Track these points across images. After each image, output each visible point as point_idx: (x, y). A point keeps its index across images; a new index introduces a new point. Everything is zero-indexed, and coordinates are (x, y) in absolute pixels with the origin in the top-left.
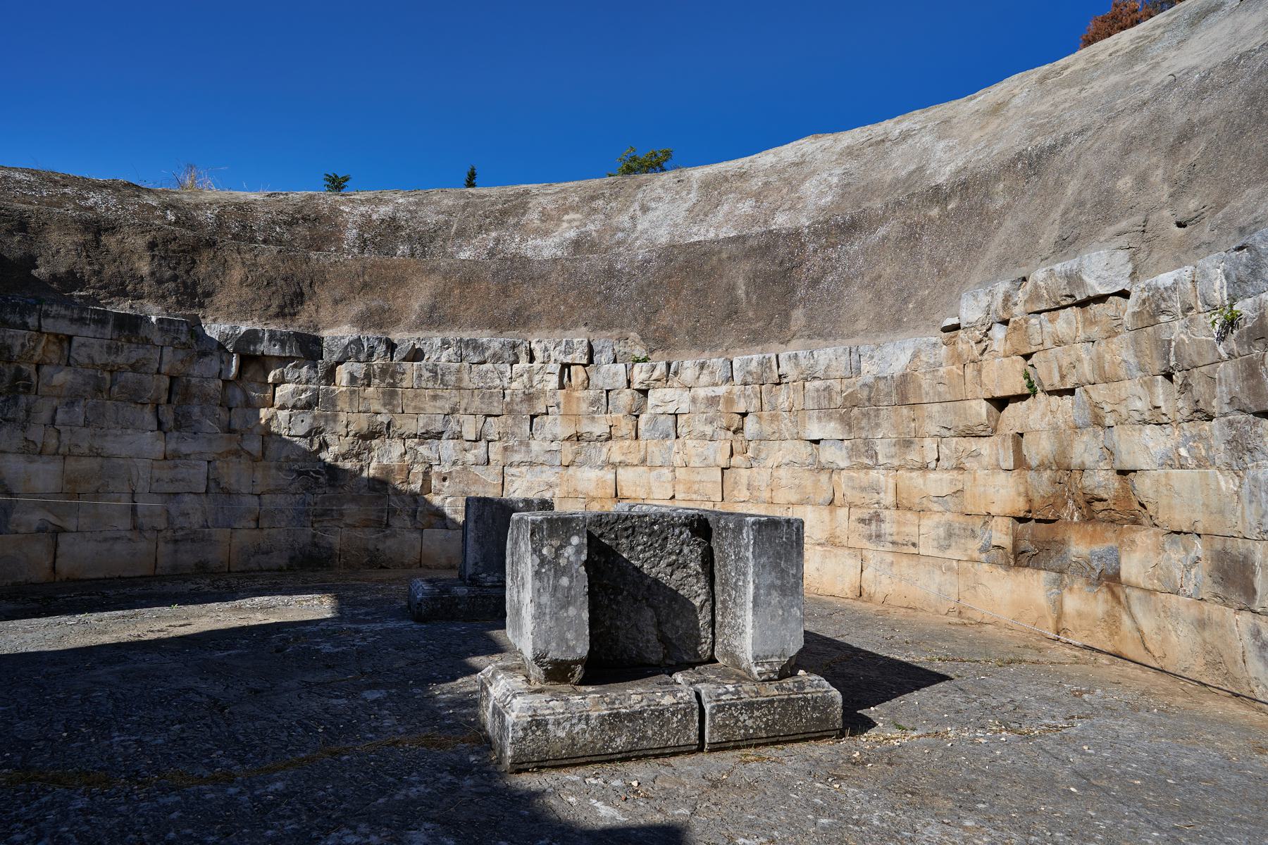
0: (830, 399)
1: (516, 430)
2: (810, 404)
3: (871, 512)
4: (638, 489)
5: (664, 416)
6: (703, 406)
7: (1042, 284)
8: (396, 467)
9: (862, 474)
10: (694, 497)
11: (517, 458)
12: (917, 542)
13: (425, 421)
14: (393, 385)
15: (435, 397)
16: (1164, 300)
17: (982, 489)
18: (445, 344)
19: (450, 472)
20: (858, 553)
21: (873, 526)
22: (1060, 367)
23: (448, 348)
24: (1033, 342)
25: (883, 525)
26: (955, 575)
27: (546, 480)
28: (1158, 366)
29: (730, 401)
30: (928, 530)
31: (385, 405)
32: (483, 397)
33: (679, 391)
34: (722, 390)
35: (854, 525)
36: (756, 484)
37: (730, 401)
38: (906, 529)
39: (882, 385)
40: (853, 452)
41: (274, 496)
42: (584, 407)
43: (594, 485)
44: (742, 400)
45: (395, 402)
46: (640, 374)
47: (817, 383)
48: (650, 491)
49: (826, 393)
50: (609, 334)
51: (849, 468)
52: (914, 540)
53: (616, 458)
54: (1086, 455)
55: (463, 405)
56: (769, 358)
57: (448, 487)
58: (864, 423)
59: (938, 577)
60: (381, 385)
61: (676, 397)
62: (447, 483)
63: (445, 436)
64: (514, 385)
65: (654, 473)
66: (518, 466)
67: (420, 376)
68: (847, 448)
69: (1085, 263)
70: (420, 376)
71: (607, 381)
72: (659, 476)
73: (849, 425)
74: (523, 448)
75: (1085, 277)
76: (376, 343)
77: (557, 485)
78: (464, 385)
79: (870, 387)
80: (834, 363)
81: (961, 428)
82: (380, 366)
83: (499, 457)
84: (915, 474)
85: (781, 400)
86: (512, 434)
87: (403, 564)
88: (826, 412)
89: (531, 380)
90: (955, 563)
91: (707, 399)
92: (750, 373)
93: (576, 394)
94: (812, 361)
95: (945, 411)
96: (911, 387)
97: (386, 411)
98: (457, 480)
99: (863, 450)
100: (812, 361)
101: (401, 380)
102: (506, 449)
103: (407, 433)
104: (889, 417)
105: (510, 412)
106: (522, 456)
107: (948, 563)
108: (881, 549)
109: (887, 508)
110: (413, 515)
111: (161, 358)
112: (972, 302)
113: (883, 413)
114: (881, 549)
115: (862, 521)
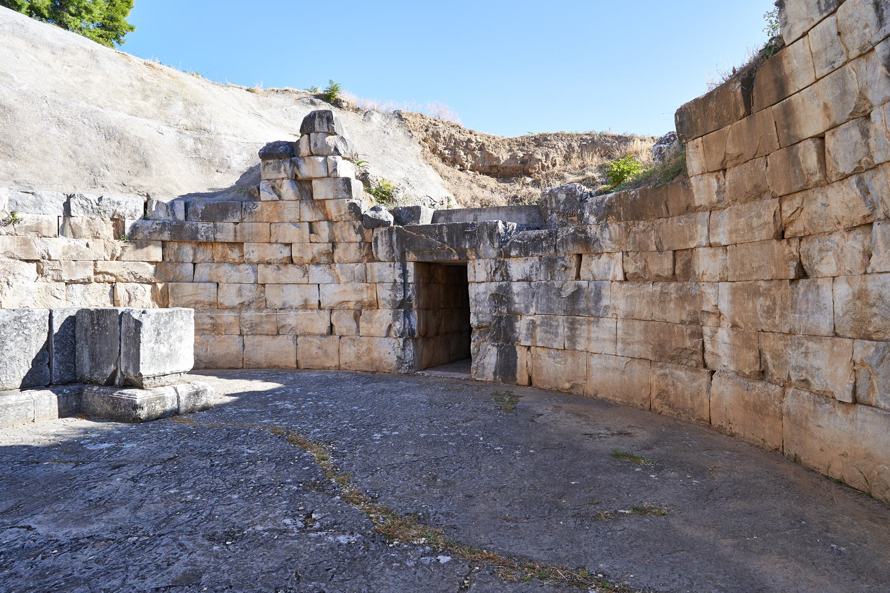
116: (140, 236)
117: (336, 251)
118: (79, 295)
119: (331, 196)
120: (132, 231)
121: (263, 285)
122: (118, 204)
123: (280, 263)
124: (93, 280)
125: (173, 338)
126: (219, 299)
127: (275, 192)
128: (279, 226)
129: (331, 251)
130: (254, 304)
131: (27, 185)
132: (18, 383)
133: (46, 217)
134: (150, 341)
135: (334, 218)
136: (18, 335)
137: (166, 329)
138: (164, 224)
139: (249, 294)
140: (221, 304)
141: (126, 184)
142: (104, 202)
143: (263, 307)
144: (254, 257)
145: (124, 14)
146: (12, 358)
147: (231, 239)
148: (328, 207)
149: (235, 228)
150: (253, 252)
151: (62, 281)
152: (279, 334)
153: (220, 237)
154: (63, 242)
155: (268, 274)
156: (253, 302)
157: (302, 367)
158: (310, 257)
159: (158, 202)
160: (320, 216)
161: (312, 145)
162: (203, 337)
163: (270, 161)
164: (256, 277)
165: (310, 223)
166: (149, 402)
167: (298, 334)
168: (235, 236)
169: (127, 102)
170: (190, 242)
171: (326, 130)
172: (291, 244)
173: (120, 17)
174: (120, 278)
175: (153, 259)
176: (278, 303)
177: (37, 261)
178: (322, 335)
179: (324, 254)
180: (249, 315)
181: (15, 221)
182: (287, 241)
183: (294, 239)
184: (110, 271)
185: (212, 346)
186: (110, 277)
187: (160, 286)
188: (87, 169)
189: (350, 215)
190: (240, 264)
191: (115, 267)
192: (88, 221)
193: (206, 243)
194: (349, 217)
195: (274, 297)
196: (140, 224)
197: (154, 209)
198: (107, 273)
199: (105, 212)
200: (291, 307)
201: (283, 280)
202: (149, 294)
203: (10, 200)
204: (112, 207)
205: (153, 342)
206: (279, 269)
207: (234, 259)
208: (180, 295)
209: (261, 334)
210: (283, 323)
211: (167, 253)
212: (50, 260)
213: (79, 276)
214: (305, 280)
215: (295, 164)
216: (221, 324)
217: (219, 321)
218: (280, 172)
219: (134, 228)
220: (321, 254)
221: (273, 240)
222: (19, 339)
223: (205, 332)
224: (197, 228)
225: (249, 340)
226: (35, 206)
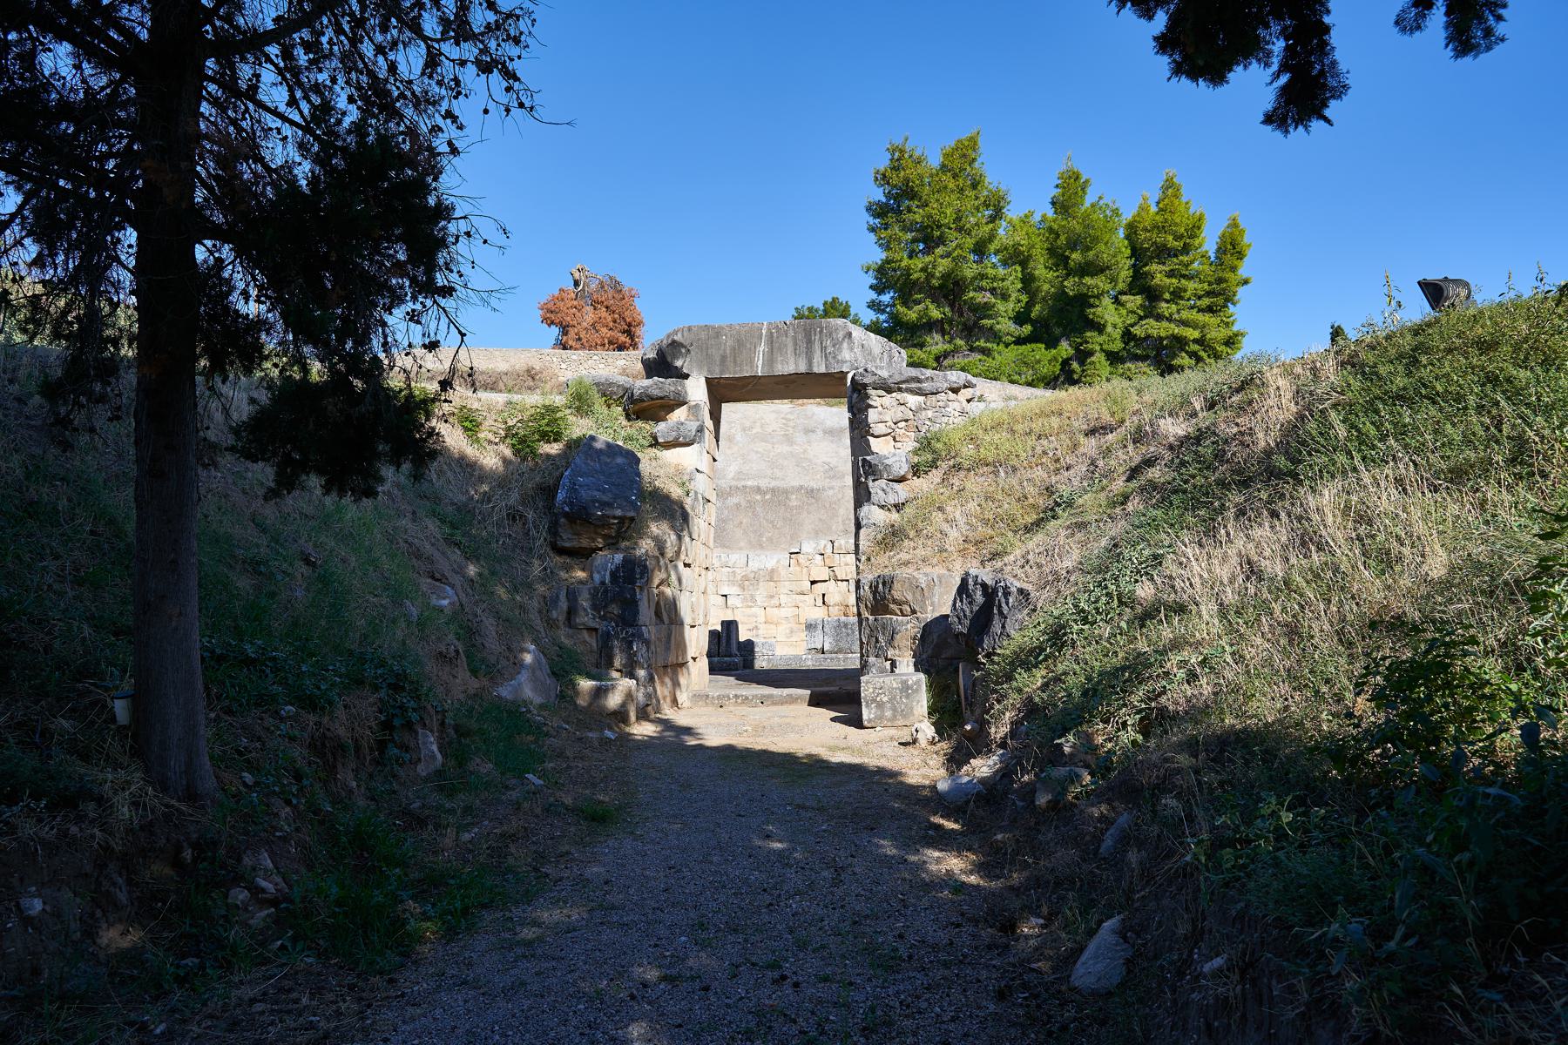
2: (724, 578)
9: (748, 609)
40: (745, 600)
58: (751, 588)
88: (732, 582)
111: (857, 546)
113: (761, 584)
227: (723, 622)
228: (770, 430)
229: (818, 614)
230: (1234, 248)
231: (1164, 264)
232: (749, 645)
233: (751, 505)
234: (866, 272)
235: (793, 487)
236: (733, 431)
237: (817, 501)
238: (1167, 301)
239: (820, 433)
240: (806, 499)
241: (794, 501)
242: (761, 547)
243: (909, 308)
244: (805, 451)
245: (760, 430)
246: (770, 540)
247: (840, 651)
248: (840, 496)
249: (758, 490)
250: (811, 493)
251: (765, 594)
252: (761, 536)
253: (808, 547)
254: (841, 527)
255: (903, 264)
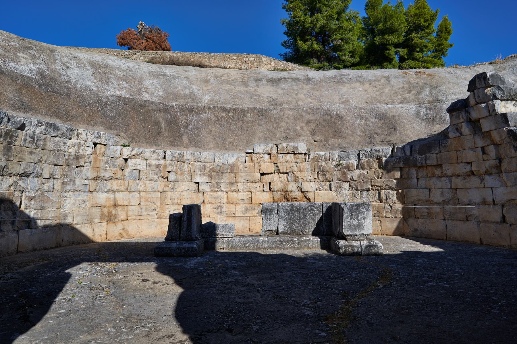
0: (205, 169)
1: (69, 173)
3: (218, 205)
4: (125, 201)
5: (135, 171)
6: (154, 168)
7: (285, 147)
8: (7, 194)
9: (215, 193)
10: (149, 203)
11: (68, 188)
12: (235, 213)
13: (25, 166)
14: (10, 143)
15: (31, 153)
16: (321, 157)
17: (258, 197)
18: (40, 124)
19: (35, 196)
20: (214, 219)
21: (219, 210)
22: (287, 167)
23: (41, 126)
24: (279, 160)
25: (222, 209)
26: (249, 221)
27: (82, 199)
28: (317, 170)
29: (165, 166)
30: (239, 210)
31: (4, 155)
32: (55, 155)
33: (142, 161)
34: (162, 162)
35: (212, 210)
36: (173, 198)
37: (165, 166)
38: (231, 210)
39: (225, 166)
40: (212, 186)
41: (342, 206)
42: (102, 164)
43: (105, 200)
44: (170, 166)
45: (10, 154)
46: (126, 152)
47: (200, 163)
48: (130, 202)
49: (203, 167)
50: (112, 132)
51: (210, 192)
52: (234, 212)
53: (115, 188)
54: (293, 188)
55: (45, 159)
56: (183, 153)
57: (34, 204)
59: (242, 222)
60: (4, 142)
61: (141, 163)
62: (33, 202)
63: (32, 176)
64: (71, 150)
65: (131, 194)
66: (68, 192)
67: (26, 140)
68: (210, 185)
69: (299, 145)
70: (26, 140)
71: (112, 153)
72: (134, 196)
73: (212, 178)
74: (72, 183)
75: (299, 148)
76: (4, 116)
77: (88, 201)
78: (47, 147)
79: (220, 167)
80: (208, 158)
81: (252, 180)
82: (5, 130)
83: (60, 187)
84: (234, 193)
85: (185, 168)
86: (67, 176)
87: (8, 253)
88: (203, 173)
89: (79, 149)
90: (248, 218)
91: (156, 165)
92: (175, 157)
93: (99, 158)
94: (200, 156)
95: (247, 175)
96: (235, 168)
97: (4, 159)
98: (38, 200)
99: (216, 186)
100: (200, 156)
101: (15, 141)
102: (63, 183)
103: (14, 173)
104: (226, 176)
105: (67, 164)
106: (71, 187)
107: (246, 218)
108: (222, 216)
109: (224, 204)
110: (13, 223)
112: (259, 147)
113: (225, 175)
114: (222, 216)
115: (215, 208)
116: (389, 166)
117: (503, 164)
118: (365, 196)
119: (493, 128)
120: (386, 164)
121: (456, 189)
122: (379, 151)
123: (466, 175)
124: (371, 189)
125: (360, 217)
126: (431, 198)
127: (458, 132)
128: (463, 152)
129: (498, 164)
130: (451, 201)
131: (344, 148)
132: (311, 233)
133: (351, 161)
134: (348, 218)
135: (498, 142)
136: (311, 213)
137: (356, 212)
138: (400, 158)
139: (447, 195)
140: (432, 201)
141: (384, 141)
142: (373, 151)
143: (457, 203)
144: (449, 172)
145: (446, 39)
146: (309, 222)
147: (435, 163)
148: (493, 136)
149: (437, 156)
150: (448, 169)
151: (359, 190)
152: (468, 220)
153: (429, 162)
154: (358, 172)
155: (458, 182)
156: (450, 200)
157: (484, 244)
158: (485, 170)
159: (397, 147)
160: (489, 142)
161: (476, 97)
162: (423, 219)
163: (453, 114)
164: (451, 184)
165: (483, 148)
166: (345, 246)
167: (481, 221)
168: (437, 161)
169: (399, 97)
170: (414, 167)
171: (484, 85)
172: (471, 162)
173: (444, 42)
174: (382, 188)
175: (396, 177)
176: (466, 201)
177: (349, 181)
178: (497, 223)
179: (494, 167)
180: (449, 207)
181: (340, 164)
182: (468, 161)
183: (473, 160)
184: (377, 184)
185: (428, 225)
186: (378, 188)
187: (400, 191)
188: (369, 136)
189: (510, 138)
190: (442, 177)
191: (379, 182)
192: (367, 161)
193: (423, 167)
194: (509, 140)
195: (463, 196)
196: (389, 160)
197: (395, 151)
198: (376, 186)
199: (373, 156)
200: (475, 204)
201: (468, 185)
202: (395, 195)
203: (338, 156)
204: (376, 153)
205: (349, 219)
206: (465, 179)
207: (438, 175)
208: (410, 196)
209: (456, 220)
210: (470, 213)
211: (403, 174)
212: (353, 180)
213: (365, 188)
214: (482, 185)
215: (467, 112)
216: (433, 213)
217: (432, 211)
218: (460, 119)
219: (386, 161)
220: (492, 167)
221: (459, 161)
222: (311, 214)
223: (424, 217)
224: (416, 159)
225: (450, 223)
226: (347, 157)
227: (171, 215)
228: (233, 78)
229: (265, 198)
230: (446, 30)
231: (418, 34)
232: (211, 228)
233: (219, 119)
234: (283, 24)
235: (248, 108)
236: (209, 77)
237: (265, 117)
238: (418, 52)
239: (265, 81)
240: (257, 116)
241: (249, 117)
242: (225, 148)
243: (305, 42)
244: (256, 90)
245: (226, 78)
246: (232, 143)
247: (292, 233)
248: (282, 114)
249: (224, 110)
250: (261, 112)
251: (227, 182)
252: (225, 140)
253: (259, 149)
254: (283, 135)
255: (302, 18)
